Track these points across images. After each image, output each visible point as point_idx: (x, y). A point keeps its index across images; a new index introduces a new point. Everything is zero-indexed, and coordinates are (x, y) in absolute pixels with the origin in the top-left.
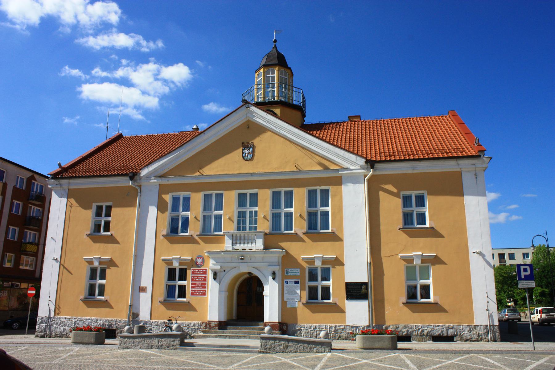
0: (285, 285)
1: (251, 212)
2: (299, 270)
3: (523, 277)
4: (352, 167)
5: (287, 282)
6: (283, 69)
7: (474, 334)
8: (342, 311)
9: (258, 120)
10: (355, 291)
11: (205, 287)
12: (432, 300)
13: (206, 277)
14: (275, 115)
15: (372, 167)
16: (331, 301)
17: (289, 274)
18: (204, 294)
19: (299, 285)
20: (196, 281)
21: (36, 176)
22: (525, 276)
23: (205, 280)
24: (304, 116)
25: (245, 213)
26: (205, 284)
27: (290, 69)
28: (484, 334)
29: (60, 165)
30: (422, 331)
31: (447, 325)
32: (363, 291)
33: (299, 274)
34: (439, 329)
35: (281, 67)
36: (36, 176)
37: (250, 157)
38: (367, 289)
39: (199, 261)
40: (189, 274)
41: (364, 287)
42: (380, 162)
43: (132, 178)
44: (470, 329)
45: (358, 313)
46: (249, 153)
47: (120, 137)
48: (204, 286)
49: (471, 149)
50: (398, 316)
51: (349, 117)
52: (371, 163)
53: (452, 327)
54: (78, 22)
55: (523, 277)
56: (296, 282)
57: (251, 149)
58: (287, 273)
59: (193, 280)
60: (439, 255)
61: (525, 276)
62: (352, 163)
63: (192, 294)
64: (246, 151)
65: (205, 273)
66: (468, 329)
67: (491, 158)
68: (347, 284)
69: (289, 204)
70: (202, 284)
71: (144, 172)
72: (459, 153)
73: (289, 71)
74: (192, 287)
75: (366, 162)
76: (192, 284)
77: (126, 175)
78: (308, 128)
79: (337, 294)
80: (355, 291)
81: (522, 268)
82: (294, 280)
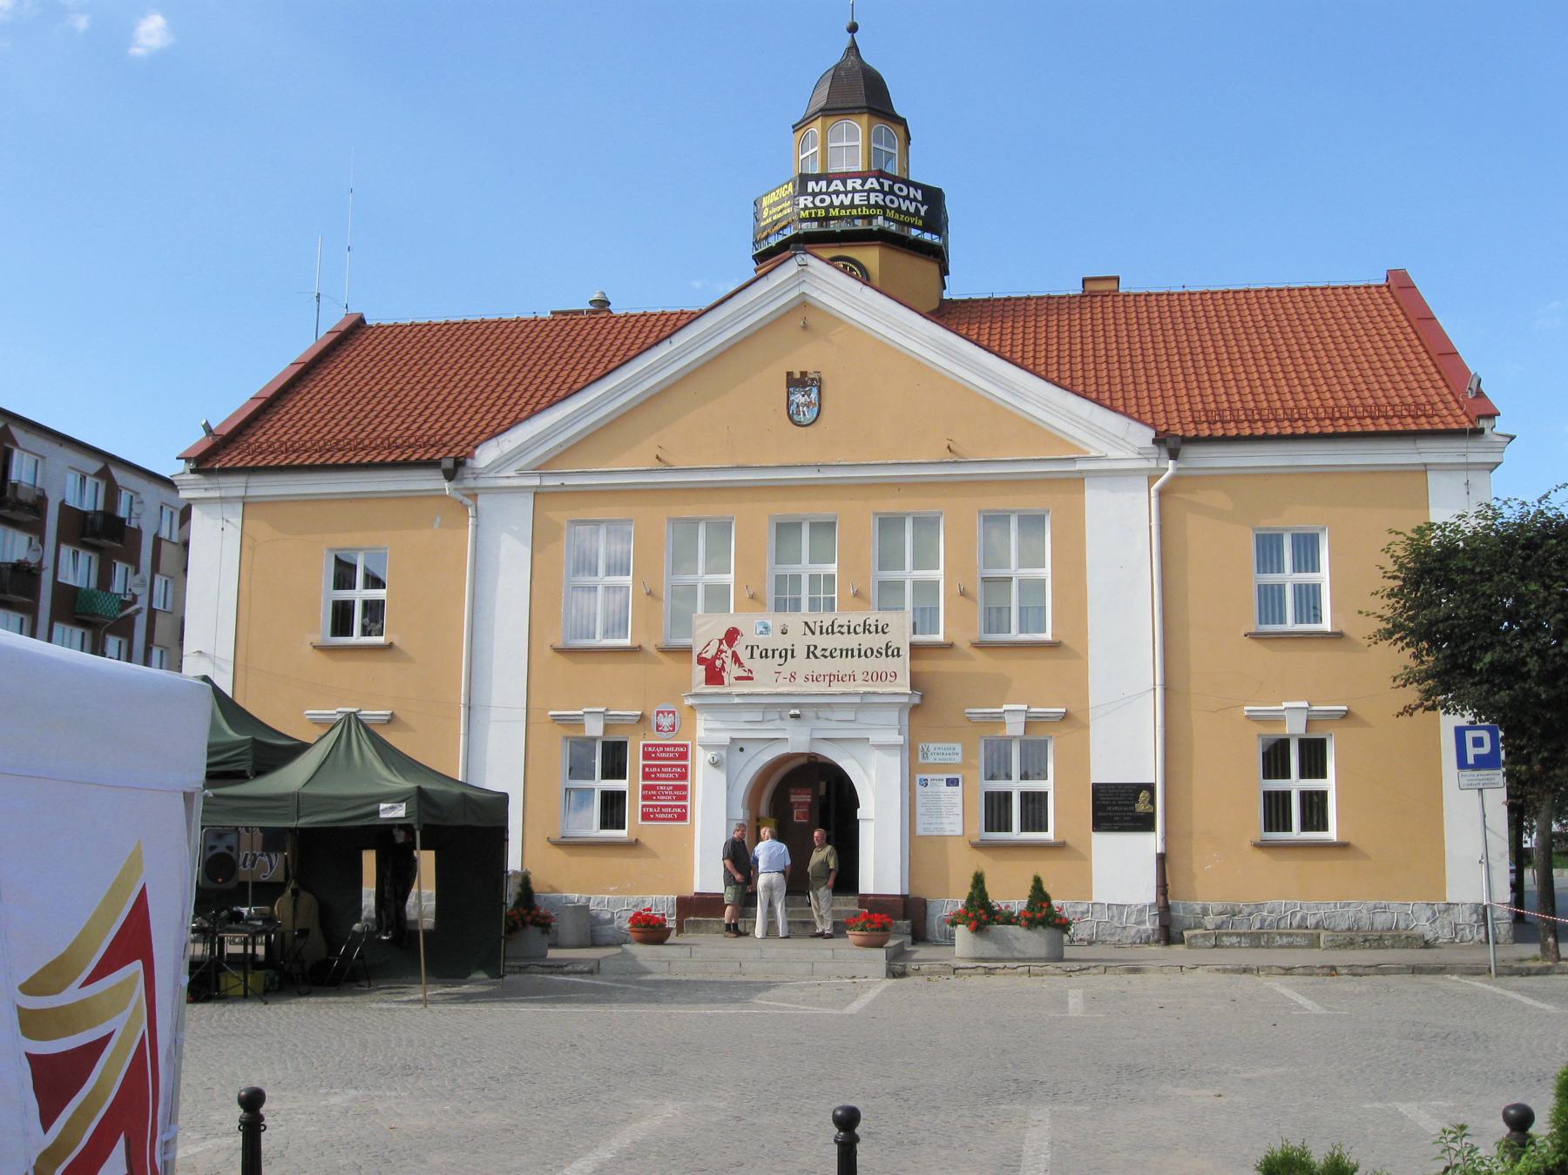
0: (919, 789)
1: (814, 579)
2: (958, 748)
3: (1471, 761)
4: (1113, 454)
5: (925, 783)
6: (881, 126)
7: (1443, 927)
8: (1084, 857)
9: (823, 298)
10: (1119, 808)
11: (684, 798)
12: (1332, 834)
13: (686, 767)
14: (865, 278)
15: (1174, 455)
16: (1049, 835)
17: (931, 760)
18: (682, 817)
19: (958, 789)
20: (657, 779)
21: (17, 432)
22: (1476, 757)
23: (683, 776)
24: (944, 271)
25: (797, 579)
26: (684, 788)
27: (902, 122)
28: (1472, 926)
29: (207, 427)
30: (1304, 919)
31: (1371, 903)
32: (1141, 807)
33: (958, 759)
34: (1351, 911)
35: (875, 120)
36: (17, 432)
37: (810, 415)
38: (1152, 801)
39: (666, 721)
40: (635, 761)
41: (1144, 795)
42: (1197, 440)
43: (450, 475)
44: (1434, 913)
45: (1121, 870)
46: (808, 405)
47: (356, 328)
48: (681, 793)
49: (1454, 405)
50: (1236, 872)
51: (1084, 281)
52: (1170, 443)
53: (1385, 909)
54: (1397, 627)
55: (1471, 761)
56: (952, 782)
57: (815, 390)
58: (925, 756)
59: (646, 776)
60: (1354, 710)
61: (1476, 757)
62: (1111, 437)
63: (646, 817)
64: (799, 398)
65: (684, 756)
66: (1429, 913)
67: (1512, 438)
68: (1097, 788)
69: (924, 559)
70: (676, 788)
71: (486, 455)
72: (1423, 420)
73: (901, 130)
74: (645, 798)
75: (1154, 441)
76: (645, 787)
77: (432, 464)
78: (947, 314)
79: (1067, 813)
80: (1119, 808)
81: (1470, 735)
82: (945, 777)
